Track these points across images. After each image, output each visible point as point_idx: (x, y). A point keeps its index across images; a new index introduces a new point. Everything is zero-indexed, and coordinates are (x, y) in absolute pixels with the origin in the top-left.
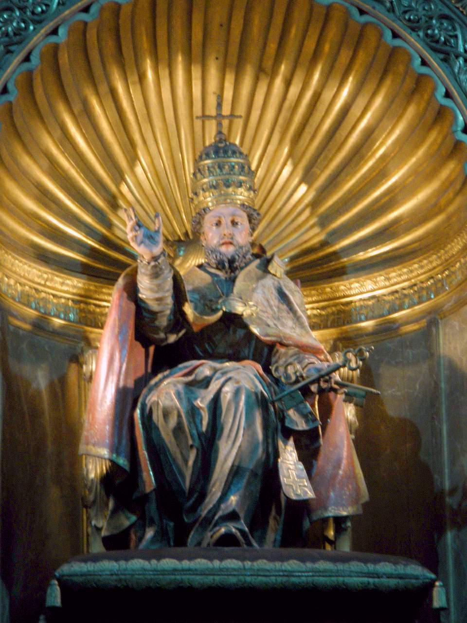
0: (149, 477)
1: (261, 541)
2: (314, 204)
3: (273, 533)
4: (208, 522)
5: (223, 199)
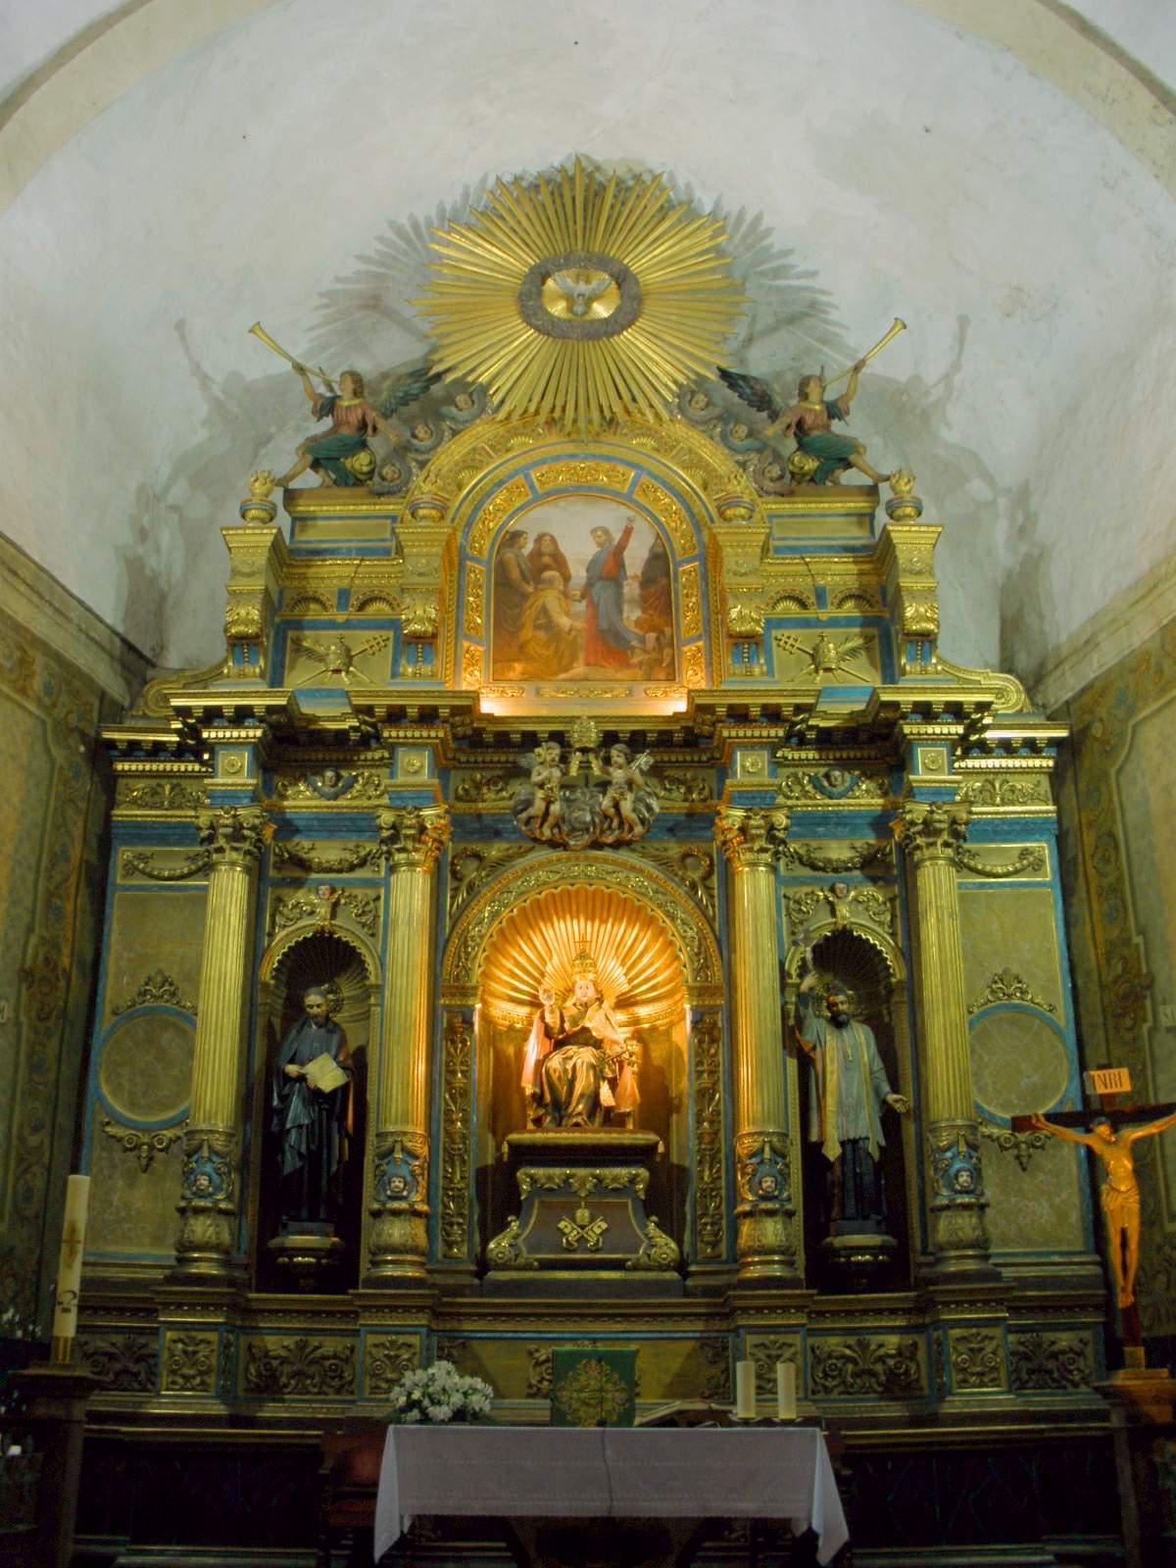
0: (548, 1097)
1: (593, 1123)
2: (626, 974)
3: (598, 1120)
4: (570, 1116)
5: (585, 978)
